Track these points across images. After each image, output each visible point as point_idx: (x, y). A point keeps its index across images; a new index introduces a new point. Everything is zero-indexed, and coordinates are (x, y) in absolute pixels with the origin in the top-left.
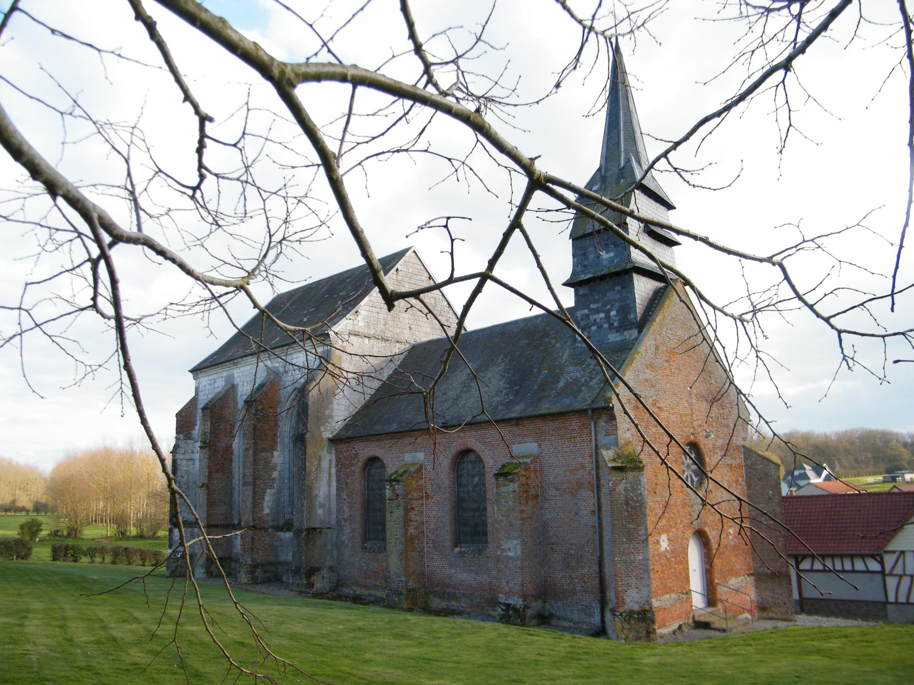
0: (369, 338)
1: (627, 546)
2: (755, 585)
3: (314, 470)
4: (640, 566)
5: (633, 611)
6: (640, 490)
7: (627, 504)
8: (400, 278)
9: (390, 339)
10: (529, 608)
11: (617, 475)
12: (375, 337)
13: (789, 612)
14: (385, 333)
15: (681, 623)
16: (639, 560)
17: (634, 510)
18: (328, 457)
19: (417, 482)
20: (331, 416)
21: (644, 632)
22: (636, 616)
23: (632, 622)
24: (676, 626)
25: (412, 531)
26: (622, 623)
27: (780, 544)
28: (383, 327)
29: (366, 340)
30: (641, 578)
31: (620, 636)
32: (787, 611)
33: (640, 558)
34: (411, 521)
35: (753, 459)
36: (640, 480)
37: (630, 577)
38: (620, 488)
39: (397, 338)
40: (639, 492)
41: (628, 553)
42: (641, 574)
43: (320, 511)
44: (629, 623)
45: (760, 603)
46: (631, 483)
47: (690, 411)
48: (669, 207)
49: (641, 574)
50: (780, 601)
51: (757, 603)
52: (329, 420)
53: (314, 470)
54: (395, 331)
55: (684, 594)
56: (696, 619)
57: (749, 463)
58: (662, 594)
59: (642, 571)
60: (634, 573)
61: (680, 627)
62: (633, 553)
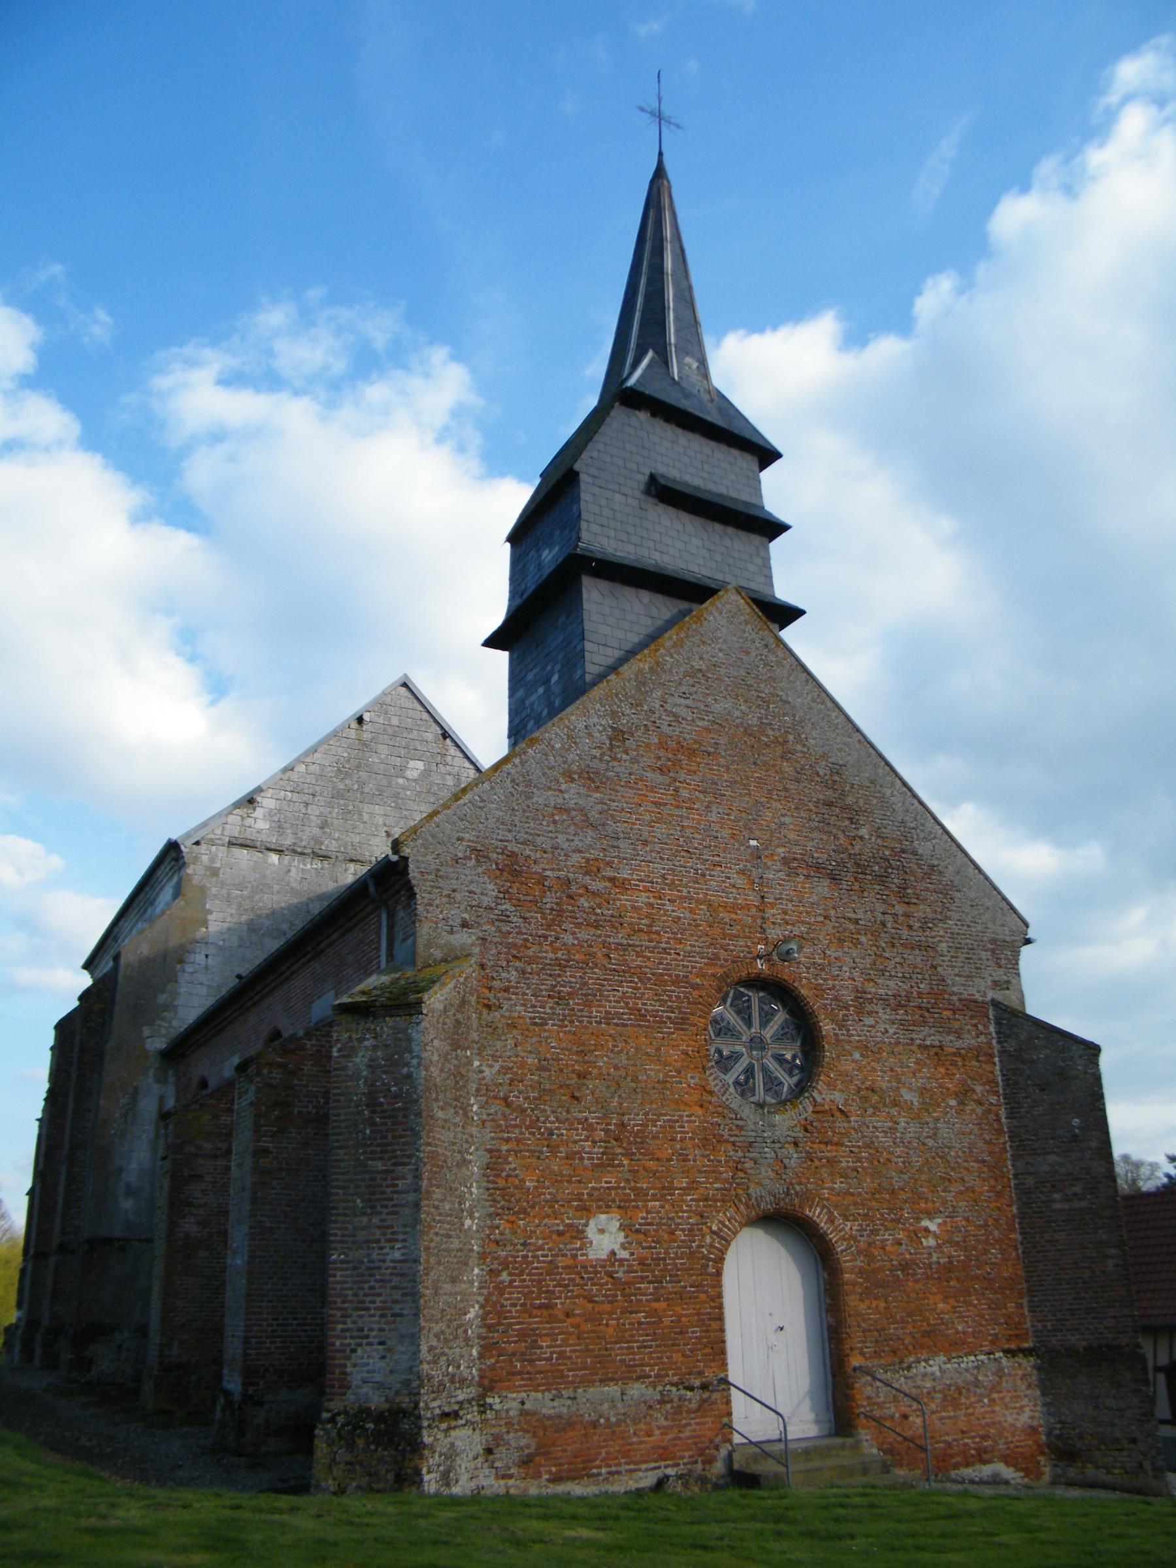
0: (279, 852)
1: (365, 1219)
2: (1041, 1381)
3: (117, 1115)
4: (396, 1280)
5: (367, 1411)
6: (407, 1064)
7: (373, 1104)
8: (366, 736)
9: (333, 855)
10: (260, 1404)
11: (354, 1026)
12: (294, 851)
13: (1147, 1465)
14: (322, 843)
15: (670, 1471)
16: (393, 1261)
17: (389, 1122)
18: (156, 1088)
19: (216, 1117)
20: (170, 1007)
21: (390, 1476)
22: (371, 1426)
23: (360, 1443)
24: (648, 1480)
25: (189, 1226)
26: (331, 1444)
27: (1110, 1263)
28: (316, 831)
29: (274, 858)
30: (393, 1315)
31: (323, 1484)
32: (1141, 1466)
33: (397, 1255)
34: (190, 1204)
35: (1024, 1036)
36: (409, 1039)
37: (368, 1309)
38: (358, 1060)
39: (352, 853)
40: (405, 1070)
41: (367, 1242)
42: (395, 1301)
43: (127, 1204)
44: (351, 1446)
45: (1059, 1437)
46: (387, 1046)
47: (753, 898)
48: (767, 456)
49: (395, 1301)
50: (1117, 1434)
51: (1049, 1434)
52: (165, 1014)
53: (117, 1115)
54: (348, 839)
55: (691, 1388)
56: (736, 1466)
57: (1011, 1045)
58: (588, 1382)
59: (397, 1295)
60: (378, 1299)
61: (660, 1484)
62: (378, 1241)
